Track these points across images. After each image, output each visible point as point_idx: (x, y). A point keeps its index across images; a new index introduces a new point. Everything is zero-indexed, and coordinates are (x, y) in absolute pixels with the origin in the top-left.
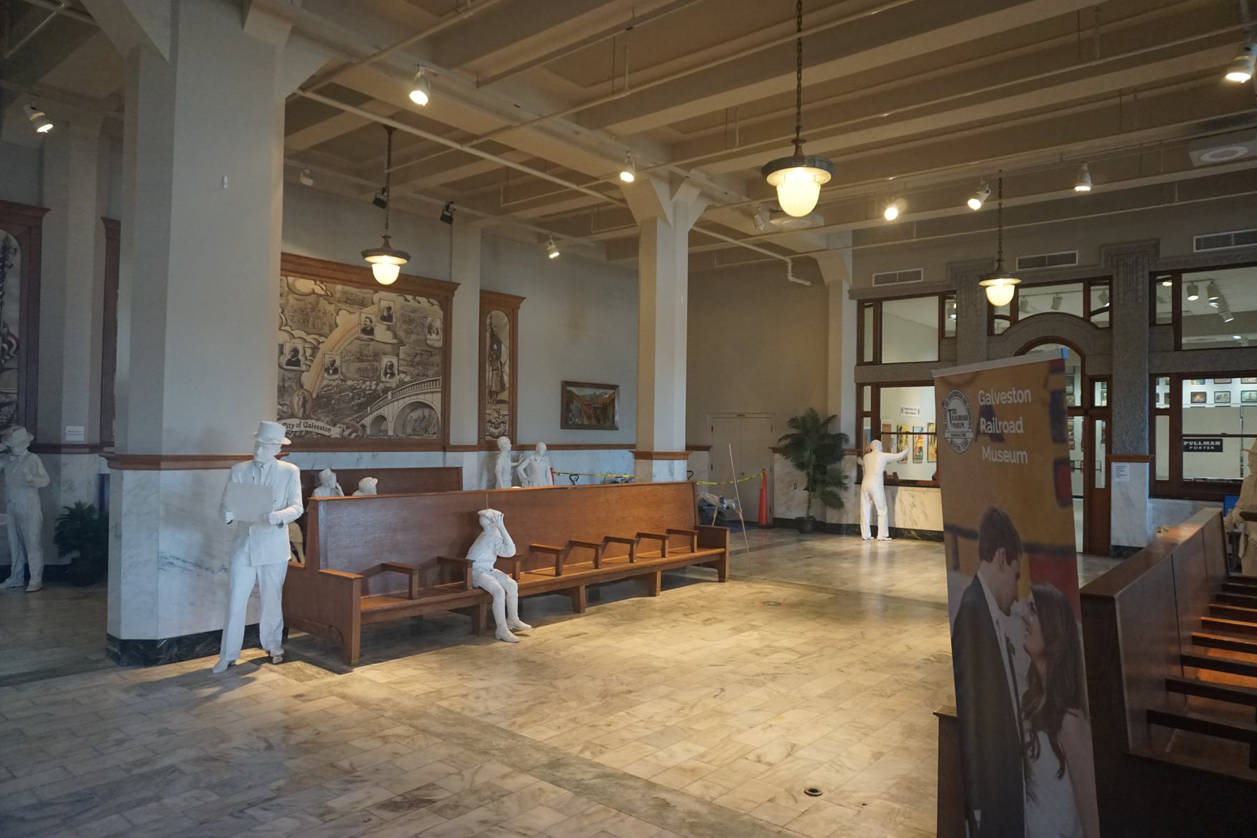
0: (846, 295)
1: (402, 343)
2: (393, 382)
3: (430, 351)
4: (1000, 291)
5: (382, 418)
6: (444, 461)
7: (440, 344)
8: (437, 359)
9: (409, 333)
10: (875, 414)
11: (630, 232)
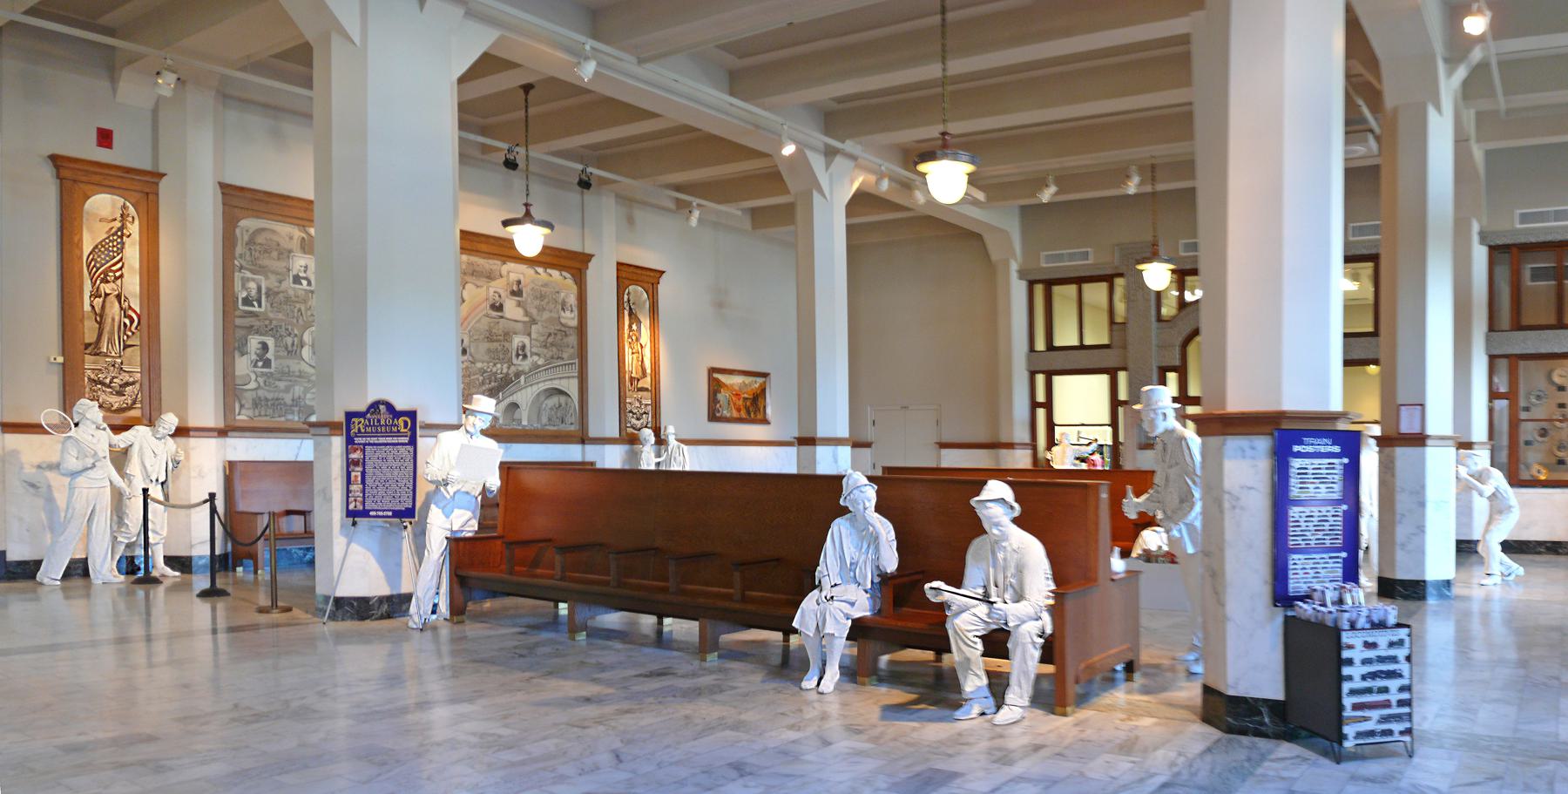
0: (1014, 275)
1: (533, 321)
2: (525, 365)
3: (563, 330)
5: (515, 406)
6: (997, 459)
7: (574, 323)
8: (573, 339)
9: (541, 309)
10: (1048, 405)
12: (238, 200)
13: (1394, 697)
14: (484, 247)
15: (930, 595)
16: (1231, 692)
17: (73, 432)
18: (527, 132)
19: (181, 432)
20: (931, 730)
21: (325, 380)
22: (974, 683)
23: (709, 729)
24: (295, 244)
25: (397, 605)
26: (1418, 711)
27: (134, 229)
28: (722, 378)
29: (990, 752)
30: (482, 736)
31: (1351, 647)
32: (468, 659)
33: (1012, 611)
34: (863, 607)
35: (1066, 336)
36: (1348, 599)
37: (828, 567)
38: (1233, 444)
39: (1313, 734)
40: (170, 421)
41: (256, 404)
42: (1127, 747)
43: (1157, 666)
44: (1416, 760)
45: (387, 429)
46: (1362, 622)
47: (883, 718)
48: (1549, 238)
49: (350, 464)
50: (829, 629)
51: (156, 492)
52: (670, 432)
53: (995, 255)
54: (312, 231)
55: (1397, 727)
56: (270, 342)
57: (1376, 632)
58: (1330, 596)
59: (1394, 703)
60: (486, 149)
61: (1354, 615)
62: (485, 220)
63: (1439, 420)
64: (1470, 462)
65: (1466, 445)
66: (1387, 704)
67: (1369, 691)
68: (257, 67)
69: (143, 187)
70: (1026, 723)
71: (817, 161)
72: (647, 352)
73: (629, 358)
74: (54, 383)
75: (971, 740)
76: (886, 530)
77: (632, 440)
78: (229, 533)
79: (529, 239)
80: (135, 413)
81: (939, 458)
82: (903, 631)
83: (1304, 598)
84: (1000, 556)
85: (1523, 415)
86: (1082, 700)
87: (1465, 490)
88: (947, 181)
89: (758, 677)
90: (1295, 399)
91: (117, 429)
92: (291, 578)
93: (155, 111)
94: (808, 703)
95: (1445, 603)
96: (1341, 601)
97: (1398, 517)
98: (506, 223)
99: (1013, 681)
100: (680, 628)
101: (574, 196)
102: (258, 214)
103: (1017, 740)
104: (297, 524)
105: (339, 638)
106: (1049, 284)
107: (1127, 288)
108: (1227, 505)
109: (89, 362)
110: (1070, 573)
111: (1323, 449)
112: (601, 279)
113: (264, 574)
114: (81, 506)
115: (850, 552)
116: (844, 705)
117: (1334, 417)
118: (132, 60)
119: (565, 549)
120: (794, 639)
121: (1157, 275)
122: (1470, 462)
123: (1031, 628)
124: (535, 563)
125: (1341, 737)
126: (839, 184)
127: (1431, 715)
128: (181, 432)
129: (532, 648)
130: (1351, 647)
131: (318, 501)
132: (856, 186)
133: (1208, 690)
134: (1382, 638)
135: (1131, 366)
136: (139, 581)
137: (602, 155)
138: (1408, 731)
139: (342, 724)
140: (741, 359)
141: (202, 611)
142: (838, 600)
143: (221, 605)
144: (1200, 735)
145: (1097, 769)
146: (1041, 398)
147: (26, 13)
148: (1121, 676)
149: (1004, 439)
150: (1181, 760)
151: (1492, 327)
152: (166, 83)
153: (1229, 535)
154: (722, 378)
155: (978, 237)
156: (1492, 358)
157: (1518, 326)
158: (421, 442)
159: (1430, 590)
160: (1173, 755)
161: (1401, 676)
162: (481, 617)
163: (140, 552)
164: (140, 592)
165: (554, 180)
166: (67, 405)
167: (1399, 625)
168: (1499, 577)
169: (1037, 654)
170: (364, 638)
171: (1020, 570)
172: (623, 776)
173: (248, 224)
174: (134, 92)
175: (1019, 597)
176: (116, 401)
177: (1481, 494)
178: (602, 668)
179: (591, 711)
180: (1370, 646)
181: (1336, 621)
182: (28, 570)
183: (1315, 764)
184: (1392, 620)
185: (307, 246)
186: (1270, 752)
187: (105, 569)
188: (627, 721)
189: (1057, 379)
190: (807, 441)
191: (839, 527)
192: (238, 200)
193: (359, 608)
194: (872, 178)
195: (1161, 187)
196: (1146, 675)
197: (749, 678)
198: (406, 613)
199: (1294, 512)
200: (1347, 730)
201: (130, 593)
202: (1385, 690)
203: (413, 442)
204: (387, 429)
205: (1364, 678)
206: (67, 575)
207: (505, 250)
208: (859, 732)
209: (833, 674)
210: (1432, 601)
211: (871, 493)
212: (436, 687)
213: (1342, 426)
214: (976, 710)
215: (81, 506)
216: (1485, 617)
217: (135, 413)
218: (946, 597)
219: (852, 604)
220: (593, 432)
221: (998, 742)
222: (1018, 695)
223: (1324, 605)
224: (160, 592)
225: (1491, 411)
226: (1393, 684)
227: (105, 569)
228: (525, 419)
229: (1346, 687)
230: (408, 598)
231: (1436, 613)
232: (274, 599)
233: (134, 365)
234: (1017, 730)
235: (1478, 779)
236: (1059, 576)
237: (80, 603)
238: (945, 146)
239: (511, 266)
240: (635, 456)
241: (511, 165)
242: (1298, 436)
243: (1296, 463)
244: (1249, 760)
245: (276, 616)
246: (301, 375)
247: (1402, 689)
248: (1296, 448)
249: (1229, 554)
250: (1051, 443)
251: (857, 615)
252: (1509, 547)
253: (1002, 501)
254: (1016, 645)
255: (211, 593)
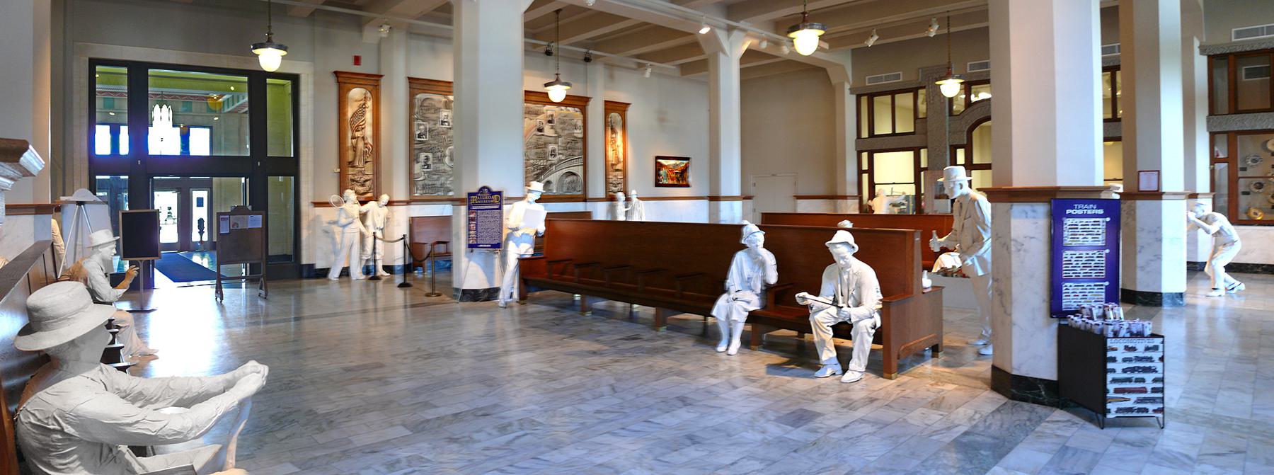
0: (847, 91)
1: (559, 136)
2: (554, 160)
3: (575, 140)
4: (951, 88)
5: (549, 182)
6: (835, 206)
7: (581, 136)
8: (580, 145)
9: (563, 129)
10: (871, 171)
11: (702, 57)
12: (416, 84)
13: (1149, 385)
14: (533, 98)
15: (799, 301)
16: (1015, 373)
17: (344, 206)
18: (557, 35)
19: (390, 203)
20: (799, 383)
21: (457, 174)
22: (828, 355)
23: (663, 375)
24: (441, 105)
25: (492, 293)
26: (1168, 392)
27: (369, 104)
28: (663, 162)
29: (839, 400)
30: (540, 372)
31: (1115, 349)
32: (528, 326)
33: (853, 313)
34: (755, 305)
35: (883, 127)
36: (1111, 314)
37: (734, 280)
38: (1018, 208)
39: (1079, 405)
40: (385, 198)
41: (424, 187)
42: (937, 404)
43: (952, 348)
44: (1166, 431)
45: (486, 202)
46: (1123, 333)
47: (768, 373)
48: (1263, 47)
49: (470, 220)
50: (734, 317)
51: (379, 234)
52: (633, 193)
53: (834, 80)
54: (451, 98)
55: (1151, 407)
56: (430, 155)
57: (1135, 340)
58: (1096, 312)
59: (1149, 390)
60: (535, 46)
61: (1117, 328)
62: (536, 84)
63: (1172, 180)
64: (1198, 209)
65: (1194, 196)
66: (1144, 390)
67: (1129, 380)
68: (426, 17)
69: (373, 82)
70: (863, 382)
71: (722, 35)
72: (621, 150)
73: (611, 153)
74: (334, 182)
75: (827, 391)
76: (770, 259)
77: (611, 198)
78: (411, 254)
79: (558, 93)
80: (369, 195)
81: (795, 206)
82: (781, 326)
83: (1075, 313)
84: (845, 277)
85: (1240, 174)
86: (901, 369)
87: (1193, 228)
88: (807, 42)
89: (690, 343)
90: (1066, 178)
91: (363, 203)
92: (441, 277)
93: (379, 45)
94: (721, 360)
95: (1179, 309)
96: (1104, 316)
97: (1138, 248)
98: (546, 85)
99: (855, 354)
100: (645, 311)
101: (581, 67)
102: (425, 91)
103: (858, 394)
104: (442, 249)
105: (465, 310)
106: (871, 97)
107: (927, 96)
108: (1013, 249)
109: (351, 171)
110: (895, 289)
111: (1089, 212)
112: (596, 110)
113: (428, 274)
114: (347, 242)
115: (747, 272)
116: (743, 362)
117: (1099, 190)
118: (369, 20)
119: (578, 266)
120: (710, 320)
121: (951, 88)
122: (1198, 209)
123: (868, 323)
124: (563, 273)
125: (1106, 411)
126: (735, 47)
127: (1173, 397)
128: (390, 203)
129: (562, 319)
130: (1115, 349)
131: (454, 239)
132: (745, 47)
133: (994, 368)
134: (1140, 345)
135: (930, 145)
136: (371, 279)
137: (597, 43)
138: (1161, 410)
139: (466, 362)
140: (680, 158)
141: (399, 295)
142: (737, 303)
143: (408, 291)
144: (990, 401)
145: (916, 418)
146: (865, 167)
147: (324, 4)
148: (929, 353)
149: (839, 193)
150: (977, 416)
151: (1212, 112)
152: (384, 31)
153: (1015, 267)
154: (663, 162)
155: (824, 70)
156: (1213, 136)
157: (1235, 109)
158: (505, 207)
159: (1165, 300)
160: (971, 412)
161: (1155, 371)
162: (536, 301)
163: (371, 263)
164: (372, 284)
165: (571, 59)
166: (341, 193)
167: (1153, 336)
168: (1223, 294)
169: (871, 339)
170: (476, 311)
171: (859, 286)
172: (617, 401)
173: (420, 96)
174: (371, 36)
175: (858, 304)
176: (361, 189)
177: (1207, 232)
178: (601, 333)
179: (596, 360)
180: (1128, 349)
181: (1102, 330)
182: (324, 273)
183: (1082, 427)
184: (1148, 332)
185: (447, 105)
186: (1047, 416)
187: (357, 273)
188: (617, 366)
189: (876, 155)
190: (714, 198)
191: (740, 257)
192: (416, 84)
193: (473, 296)
194: (756, 41)
195: (952, 30)
196: (946, 354)
197: (685, 344)
198: (496, 298)
199: (1067, 254)
200: (1109, 406)
201: (367, 286)
202: (1143, 380)
203: (500, 208)
204: (486, 202)
205: (1124, 371)
206: (341, 275)
207: (544, 98)
208: (754, 381)
209: (736, 343)
210: (1166, 308)
211: (760, 237)
212: (513, 342)
213: (1104, 196)
214: (829, 372)
215: (347, 242)
216: (1211, 321)
217: (369, 195)
218: (809, 302)
219: (748, 302)
220: (590, 195)
221: (845, 394)
222: (858, 364)
223: (1091, 318)
224: (380, 284)
225: (1212, 172)
226: (1149, 377)
227: (357, 273)
228: (554, 190)
229: (1110, 377)
230: (497, 290)
231: (1171, 317)
232: (433, 289)
233: (369, 171)
234: (857, 386)
235: (1224, 451)
236: (884, 290)
237: (346, 290)
238: (804, 20)
239: (548, 107)
240: (612, 210)
241: (548, 53)
242: (1071, 203)
243: (1069, 221)
244: (1029, 420)
245: (434, 298)
246: (445, 172)
247: (1155, 380)
248: (1068, 211)
249: (1016, 283)
250: (872, 195)
251: (752, 309)
252: (1232, 268)
253: (846, 243)
254: (857, 334)
255: (403, 286)
